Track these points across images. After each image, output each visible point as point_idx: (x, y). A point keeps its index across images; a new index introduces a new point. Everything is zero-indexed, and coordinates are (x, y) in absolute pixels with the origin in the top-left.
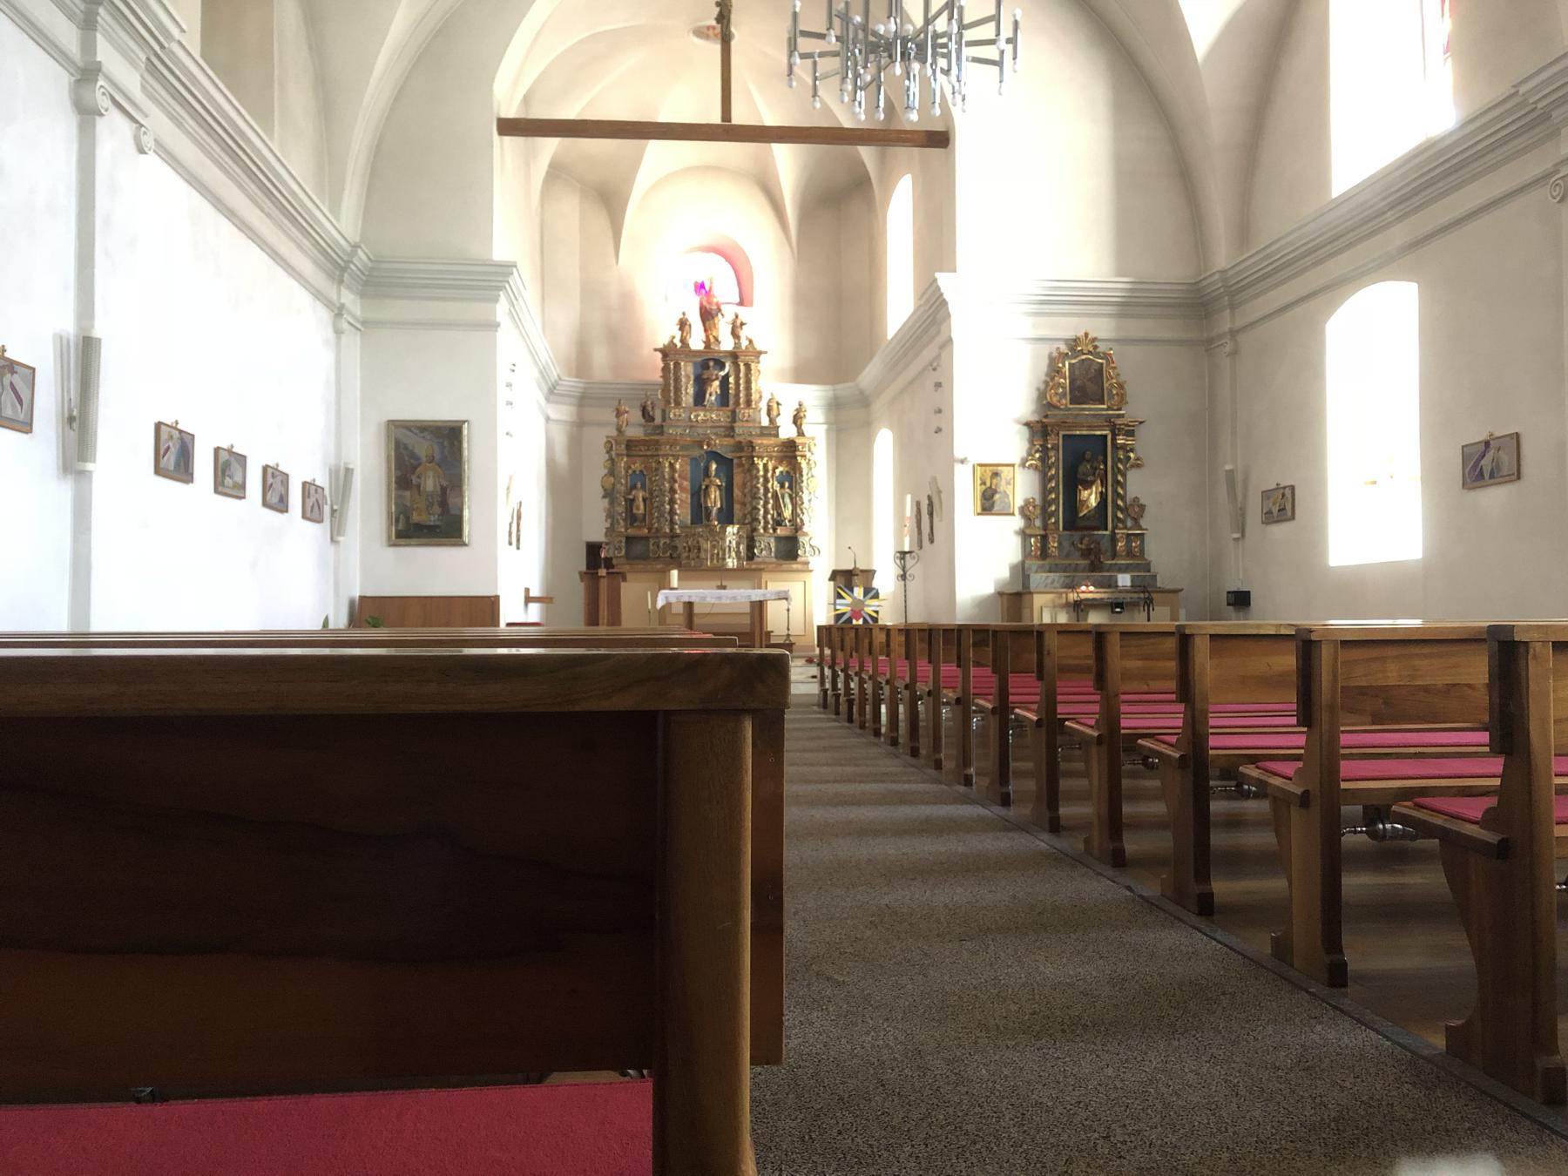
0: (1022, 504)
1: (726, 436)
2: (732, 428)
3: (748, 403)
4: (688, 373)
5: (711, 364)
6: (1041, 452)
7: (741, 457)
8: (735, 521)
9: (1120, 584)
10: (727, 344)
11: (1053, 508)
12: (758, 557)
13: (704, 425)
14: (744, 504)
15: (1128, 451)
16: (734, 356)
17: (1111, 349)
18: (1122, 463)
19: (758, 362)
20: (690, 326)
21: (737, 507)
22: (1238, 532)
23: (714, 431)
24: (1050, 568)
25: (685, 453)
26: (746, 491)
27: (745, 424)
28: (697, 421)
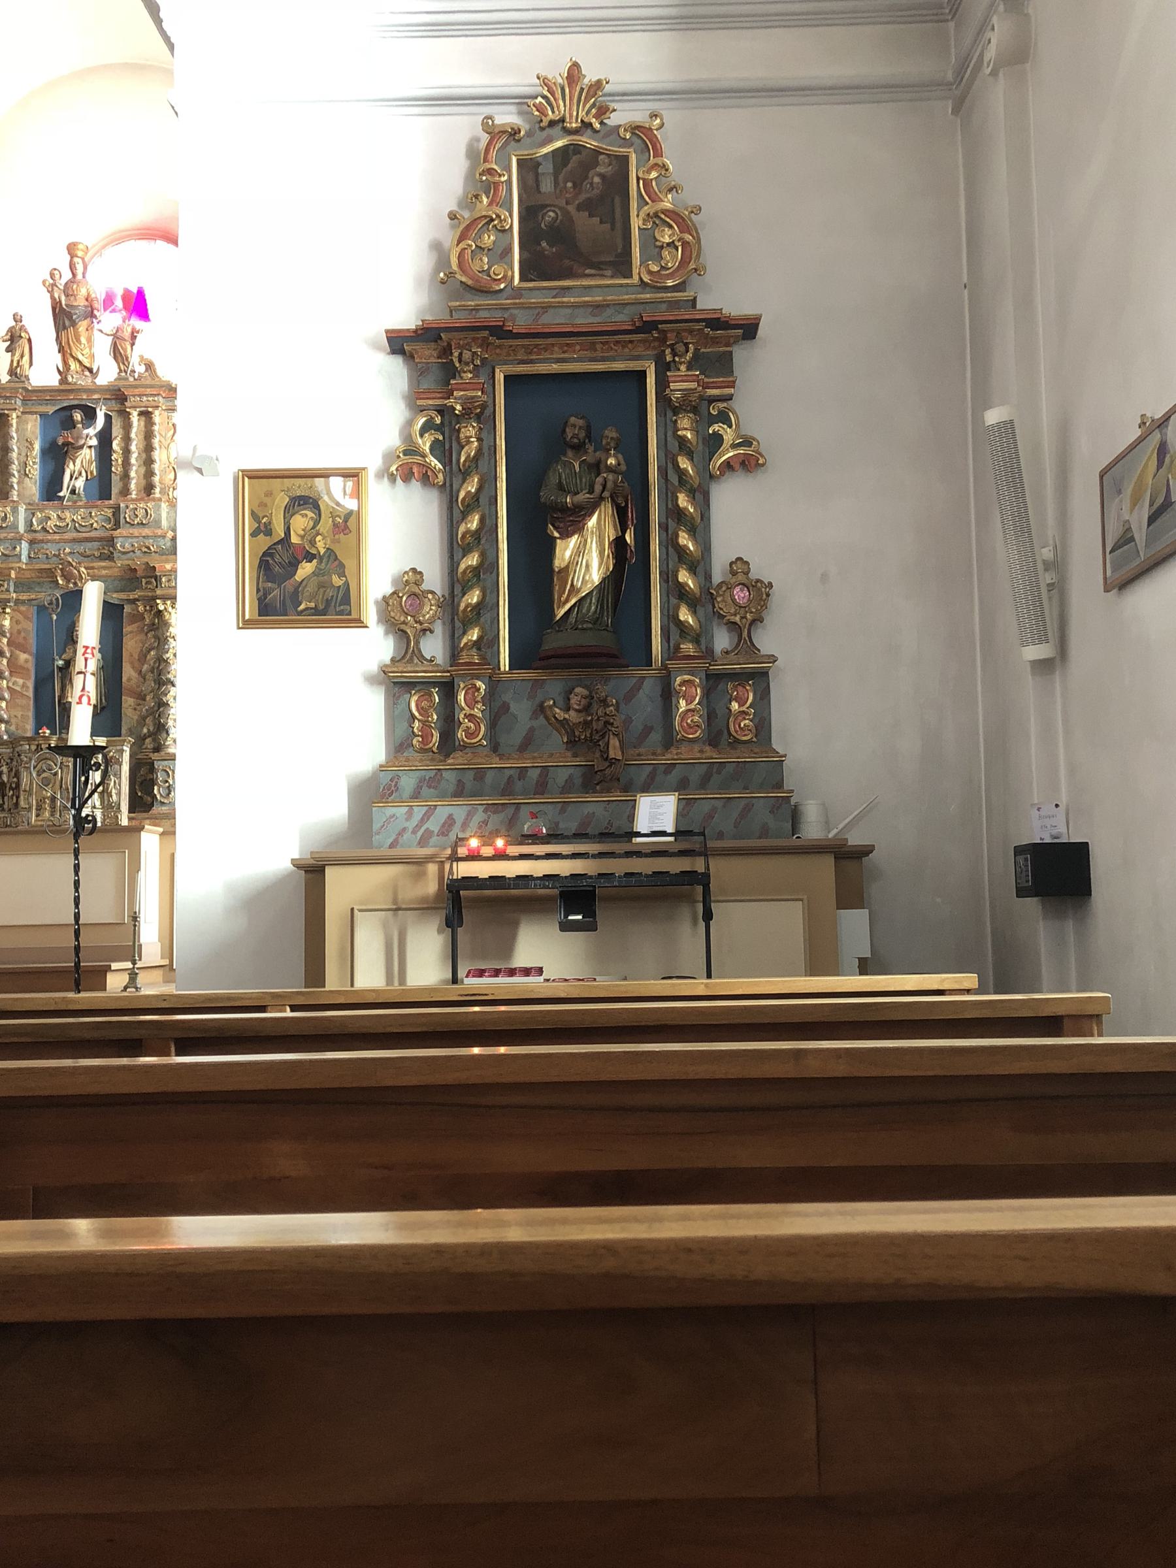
0: (388, 589)
1: (102, 558)
2: (111, 541)
3: (149, 488)
4: (29, 434)
5: (78, 416)
6: (439, 428)
7: (133, 602)
8: (124, 731)
9: (643, 823)
10: (108, 373)
11: (474, 597)
12: (163, 803)
13: (57, 537)
14: (141, 697)
15: (712, 420)
16: (118, 396)
17: (654, 116)
18: (690, 455)
19: (173, 409)
20: (30, 340)
21: (128, 702)
22: (1043, 639)
23: (80, 548)
24: (460, 783)
25: (24, 597)
26: (145, 667)
27: (135, 531)
28: (44, 529)
